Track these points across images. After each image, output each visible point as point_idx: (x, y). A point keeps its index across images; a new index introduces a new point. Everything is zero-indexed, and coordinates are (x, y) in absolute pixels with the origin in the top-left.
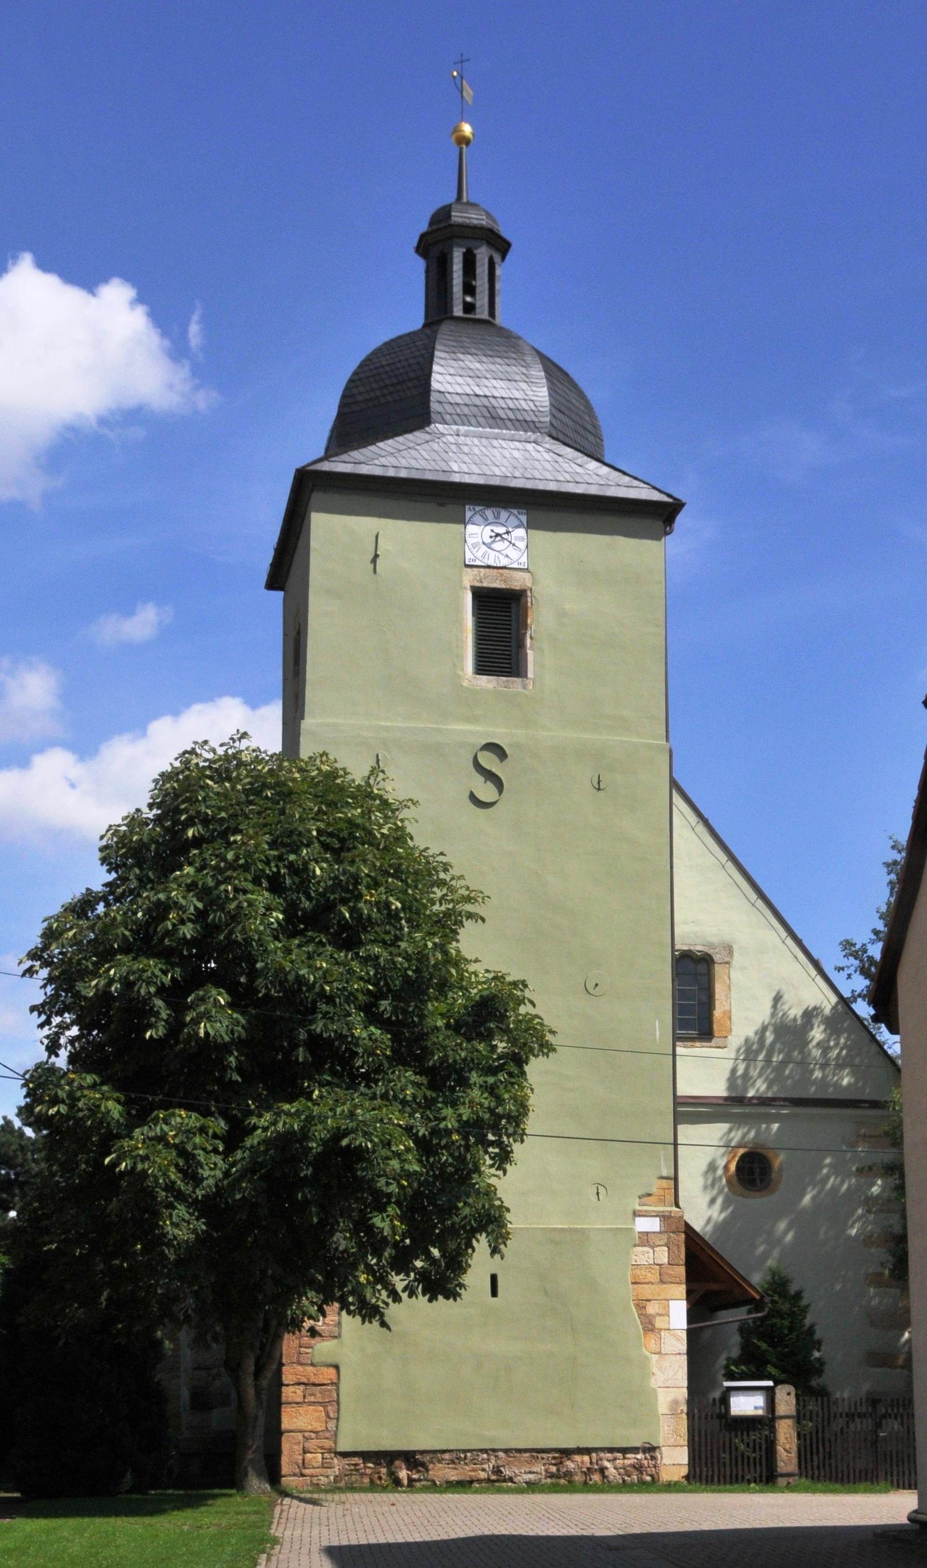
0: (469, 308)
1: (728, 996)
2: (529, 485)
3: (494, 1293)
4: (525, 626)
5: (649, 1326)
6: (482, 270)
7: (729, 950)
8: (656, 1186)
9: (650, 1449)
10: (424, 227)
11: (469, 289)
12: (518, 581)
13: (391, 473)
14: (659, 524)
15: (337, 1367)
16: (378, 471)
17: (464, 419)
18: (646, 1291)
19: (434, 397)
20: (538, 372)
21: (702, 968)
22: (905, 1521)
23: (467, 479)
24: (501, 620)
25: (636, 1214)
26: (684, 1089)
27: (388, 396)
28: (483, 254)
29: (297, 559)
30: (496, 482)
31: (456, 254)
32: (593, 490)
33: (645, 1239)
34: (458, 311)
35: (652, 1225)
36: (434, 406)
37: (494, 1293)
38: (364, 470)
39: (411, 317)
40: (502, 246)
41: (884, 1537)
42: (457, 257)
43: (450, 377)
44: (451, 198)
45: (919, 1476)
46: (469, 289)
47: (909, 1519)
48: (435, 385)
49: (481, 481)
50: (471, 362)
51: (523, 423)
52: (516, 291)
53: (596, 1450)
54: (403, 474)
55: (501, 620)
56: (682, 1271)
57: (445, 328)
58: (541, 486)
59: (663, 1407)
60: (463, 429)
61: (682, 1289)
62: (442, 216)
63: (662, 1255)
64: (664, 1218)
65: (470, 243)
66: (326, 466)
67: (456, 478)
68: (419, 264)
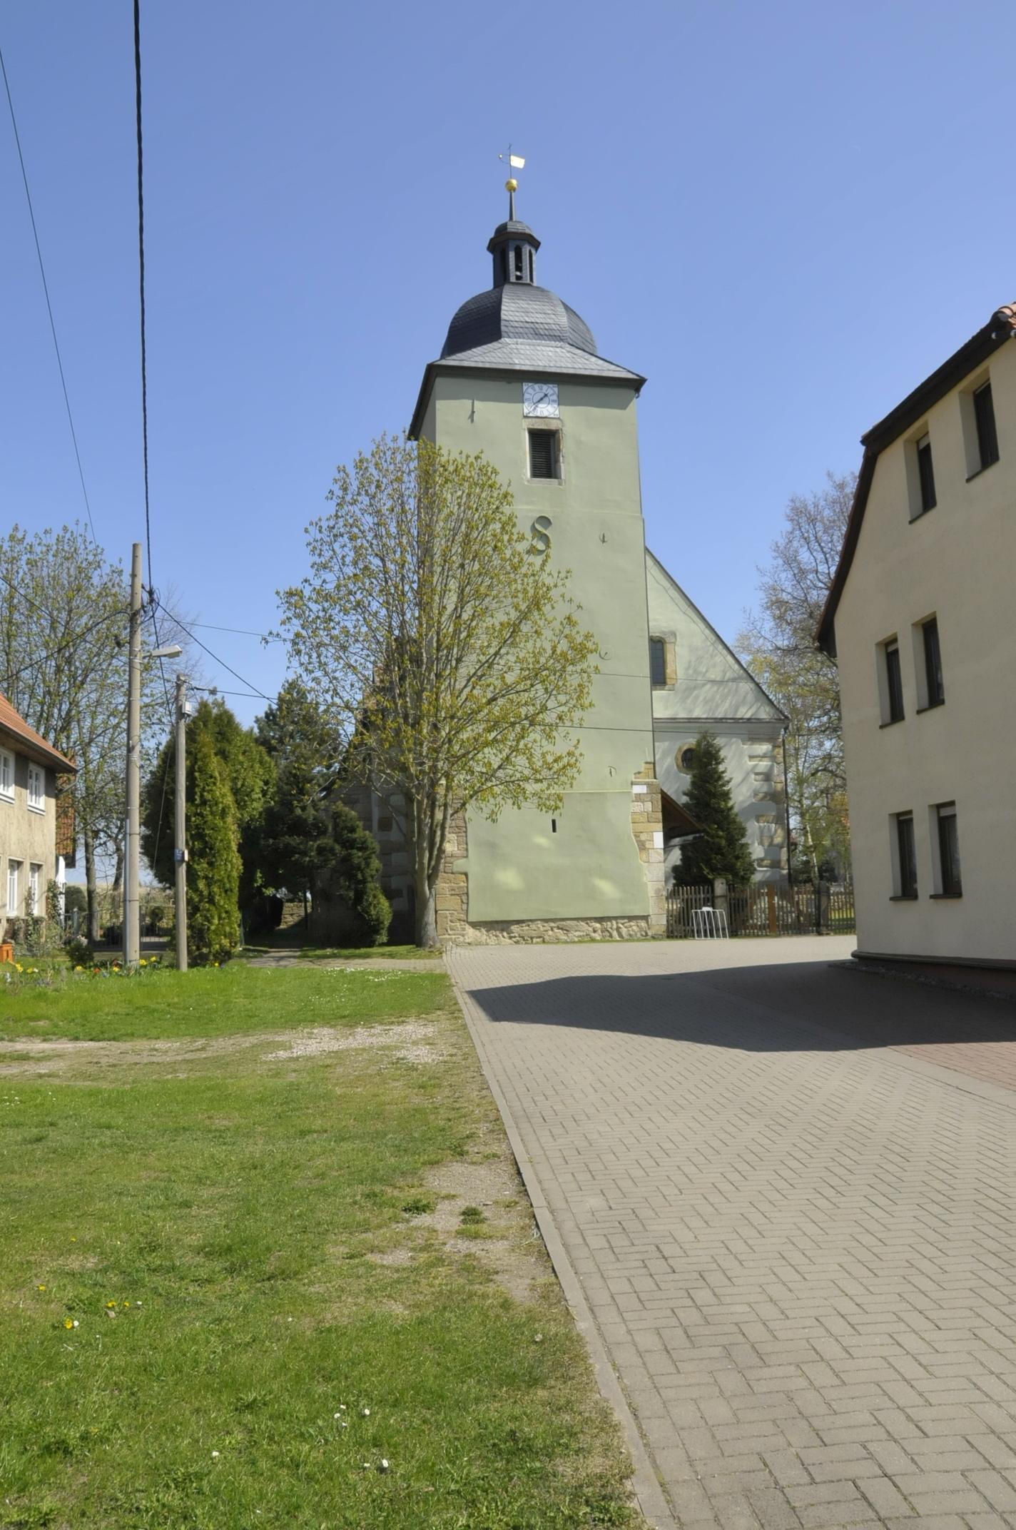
0: (519, 278)
1: (675, 661)
2: (558, 371)
3: (554, 830)
4: (559, 450)
5: (642, 846)
6: (526, 257)
7: (674, 634)
8: (643, 767)
9: (645, 918)
10: (492, 235)
11: (519, 268)
12: (553, 426)
13: (481, 365)
14: (632, 392)
15: (466, 875)
16: (473, 365)
17: (519, 335)
18: (640, 827)
19: (503, 323)
20: (561, 310)
21: (659, 645)
22: (850, 957)
23: (524, 368)
24: (545, 449)
25: (632, 784)
26: (656, 716)
27: (479, 323)
28: (526, 249)
29: (429, 409)
30: (540, 369)
31: (509, 248)
32: (595, 373)
33: (639, 798)
34: (513, 279)
35: (641, 789)
36: (503, 328)
37: (554, 830)
38: (466, 364)
39: (485, 282)
40: (536, 244)
41: (836, 968)
42: (512, 255)
43: (512, 309)
44: (505, 219)
45: (380, 960)
46: (519, 268)
47: (853, 955)
48: (503, 317)
49: (531, 369)
50: (523, 304)
51: (557, 337)
52: (543, 265)
53: (609, 919)
54: (487, 366)
55: (545, 449)
56: (660, 815)
57: (507, 289)
58: (565, 371)
59: (651, 892)
60: (520, 340)
61: (660, 825)
62: (502, 230)
63: (649, 806)
64: (648, 784)
65: (518, 243)
66: (444, 362)
67: (518, 368)
68: (490, 257)
